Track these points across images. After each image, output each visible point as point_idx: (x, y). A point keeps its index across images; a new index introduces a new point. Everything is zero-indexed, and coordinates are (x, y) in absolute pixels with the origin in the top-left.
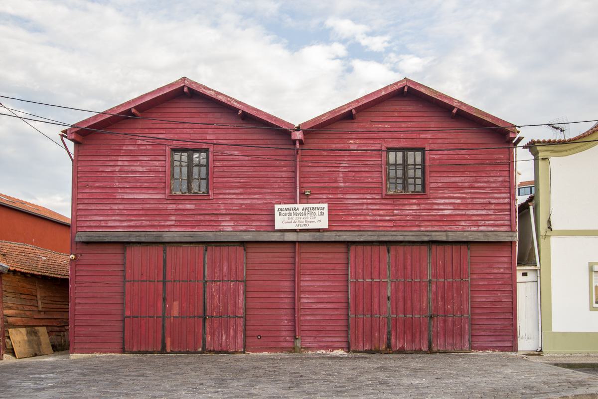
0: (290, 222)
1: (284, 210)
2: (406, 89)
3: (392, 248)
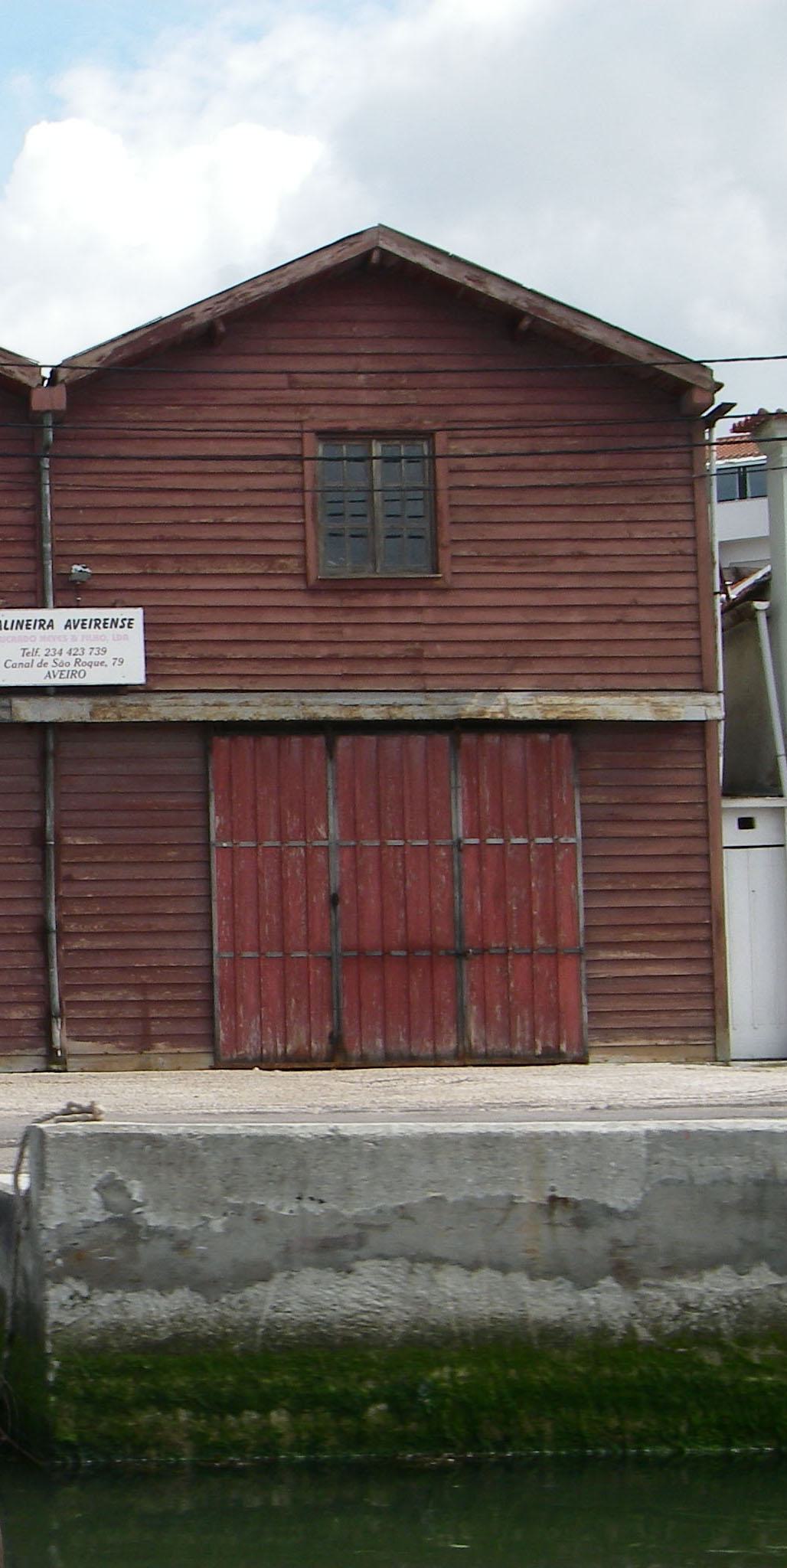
0: (27, 665)
1: (9, 625)
2: (375, 256)
3: (343, 743)
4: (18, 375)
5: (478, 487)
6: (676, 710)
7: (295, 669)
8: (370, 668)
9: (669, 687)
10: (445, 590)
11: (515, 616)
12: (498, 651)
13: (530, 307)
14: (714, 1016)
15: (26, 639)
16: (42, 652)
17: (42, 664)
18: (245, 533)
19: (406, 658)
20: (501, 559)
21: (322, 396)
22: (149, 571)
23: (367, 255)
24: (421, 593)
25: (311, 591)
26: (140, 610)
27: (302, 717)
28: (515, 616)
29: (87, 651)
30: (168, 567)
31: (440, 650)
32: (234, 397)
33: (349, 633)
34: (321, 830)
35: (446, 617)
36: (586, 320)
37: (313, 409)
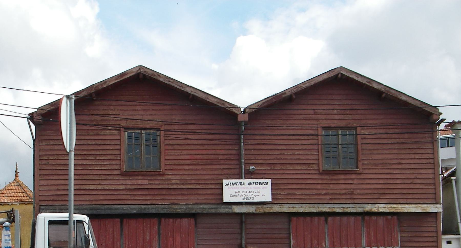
5: (370, 144)
8: (338, 197)
10: (360, 174)
11: (381, 182)
12: (376, 192)
15: (236, 188)
16: (241, 192)
17: (241, 196)
20: (376, 165)
21: (324, 117)
23: (337, 75)
25: (321, 174)
26: (270, 180)
28: (381, 182)
29: (254, 192)
31: (358, 191)
32: (298, 117)
33: (332, 186)
34: (323, 244)
35: (360, 182)
37: (321, 121)
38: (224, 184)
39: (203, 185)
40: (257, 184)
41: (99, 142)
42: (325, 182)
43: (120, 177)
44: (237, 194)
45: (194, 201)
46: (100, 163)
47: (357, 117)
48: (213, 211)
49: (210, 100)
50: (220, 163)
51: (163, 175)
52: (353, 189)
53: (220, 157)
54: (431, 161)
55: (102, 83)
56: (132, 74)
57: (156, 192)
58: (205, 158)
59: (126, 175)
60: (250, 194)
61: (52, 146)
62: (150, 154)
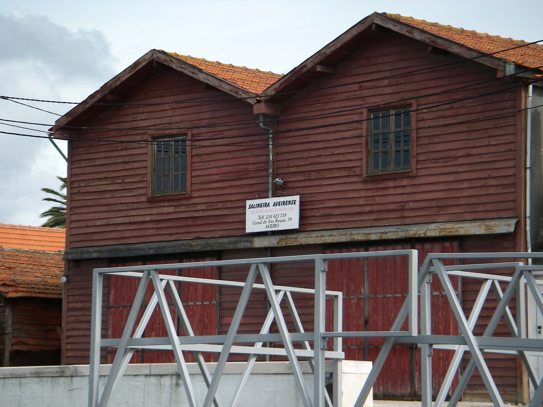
4: (487, 62)
5: (429, 127)
6: (495, 228)
7: (358, 218)
8: (385, 215)
9: (503, 216)
10: (414, 177)
11: (441, 187)
12: (434, 204)
13: (431, 41)
14: (517, 380)
15: (260, 212)
16: (265, 217)
17: (265, 222)
18: (341, 158)
19: (398, 210)
20: (436, 160)
21: (372, 92)
22: (307, 178)
23: (371, 26)
24: (405, 179)
25: (365, 182)
26: (298, 196)
27: (348, 240)
28: (441, 187)
29: (280, 216)
30: (314, 176)
31: (411, 205)
32: (339, 97)
33: (378, 200)
34: (362, 291)
35: (415, 190)
36: (453, 44)
37: (368, 98)
38: (247, 207)
39: (230, 210)
40: (259, 206)
41: (127, 159)
42: (370, 194)
43: (146, 205)
44: (260, 221)
45: (220, 234)
46: (128, 188)
47: (414, 86)
48: (231, 247)
49: (223, 88)
50: (249, 176)
51: (190, 198)
52: (405, 202)
53: (250, 167)
54: (512, 146)
55: (116, 79)
56: (144, 63)
57: (181, 223)
58: (234, 170)
59: (153, 201)
60: (274, 219)
61: (83, 169)
62: (178, 171)
